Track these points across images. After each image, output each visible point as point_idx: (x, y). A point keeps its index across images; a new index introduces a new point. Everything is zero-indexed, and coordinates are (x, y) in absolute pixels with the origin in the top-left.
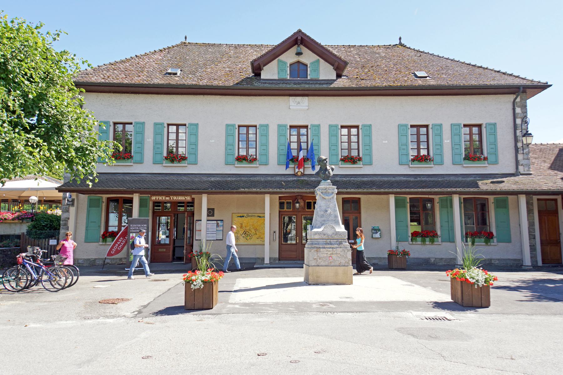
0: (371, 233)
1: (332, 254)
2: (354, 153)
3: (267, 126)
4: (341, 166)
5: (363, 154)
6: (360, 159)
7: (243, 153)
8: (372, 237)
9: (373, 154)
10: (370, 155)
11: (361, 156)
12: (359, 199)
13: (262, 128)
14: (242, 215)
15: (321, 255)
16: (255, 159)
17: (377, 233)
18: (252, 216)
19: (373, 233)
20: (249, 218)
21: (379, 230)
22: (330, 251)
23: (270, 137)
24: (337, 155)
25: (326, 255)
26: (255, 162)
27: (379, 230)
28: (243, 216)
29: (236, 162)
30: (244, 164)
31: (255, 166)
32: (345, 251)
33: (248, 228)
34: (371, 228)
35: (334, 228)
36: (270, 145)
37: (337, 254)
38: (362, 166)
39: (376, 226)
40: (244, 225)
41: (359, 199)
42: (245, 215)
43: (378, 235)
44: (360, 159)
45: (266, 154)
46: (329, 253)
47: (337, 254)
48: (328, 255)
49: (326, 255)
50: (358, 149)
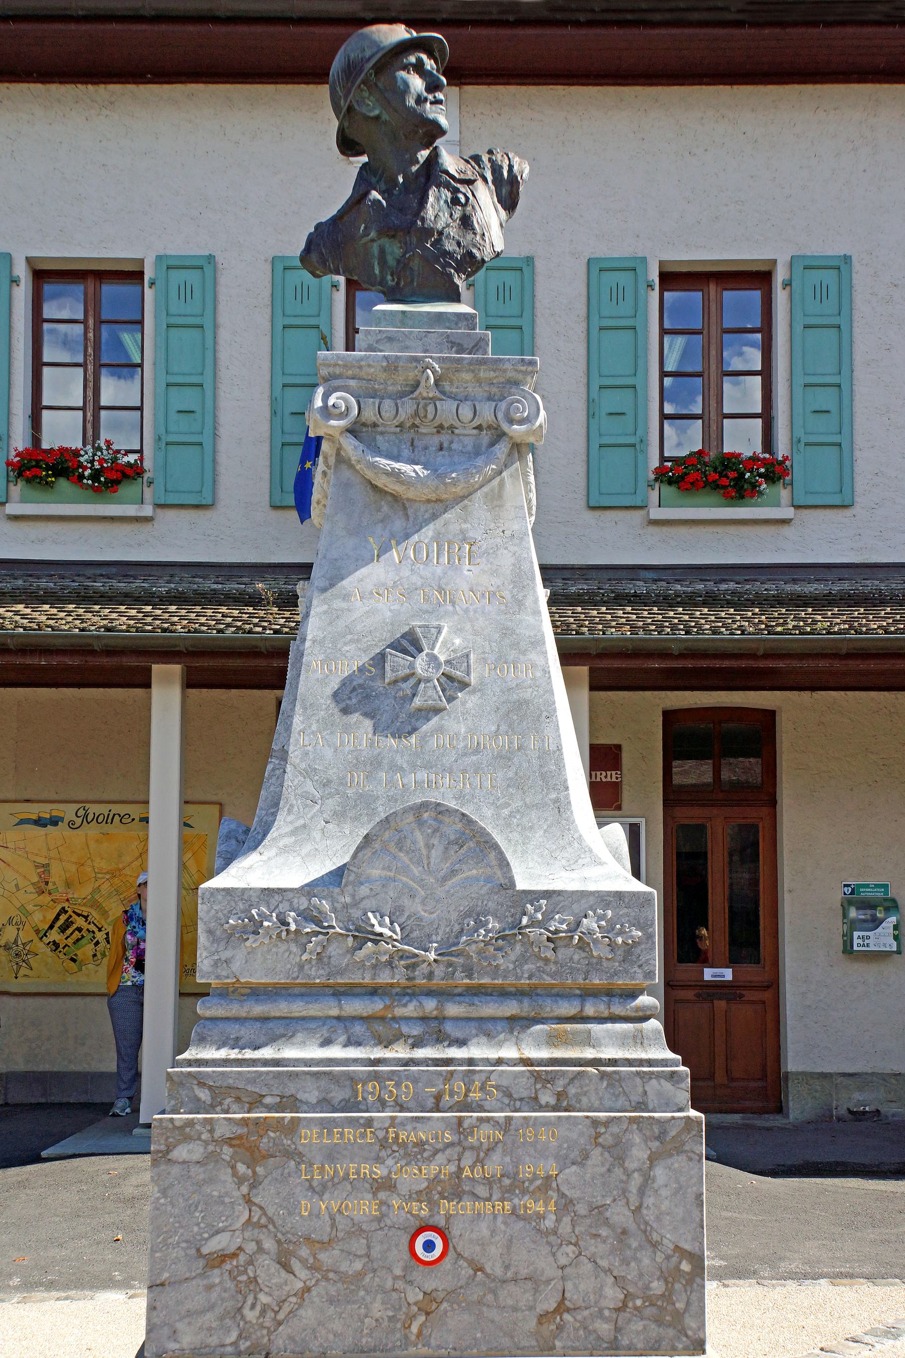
0: (838, 927)
1: (456, 1189)
2: (742, 440)
3: (205, 266)
4: (656, 513)
5: (794, 442)
6: (776, 472)
7: (62, 432)
8: (848, 949)
9: (859, 440)
10: (840, 447)
11: (782, 449)
12: (769, 717)
13: (177, 277)
14: (45, 811)
15: (310, 1212)
16: (134, 472)
17: (876, 923)
18: (109, 819)
19: (854, 925)
20: (92, 831)
21: (892, 906)
22: (418, 1152)
23: (224, 335)
24: (637, 447)
25: (364, 1207)
26: (127, 490)
27: (892, 906)
28: (54, 822)
29: (17, 490)
30: (65, 501)
31: (130, 510)
32: (618, 1152)
33: (85, 891)
34: (838, 896)
35: (486, 846)
36: (224, 389)
37: (513, 1186)
38: (788, 512)
39: (871, 879)
40: (57, 875)
41: (769, 717)
42: (68, 811)
43: (882, 938)
44: (776, 472)
45: (197, 439)
46: (413, 1177)
47: (513, 1186)
48: (404, 1210)
49: (364, 1207)
50: (767, 416)
